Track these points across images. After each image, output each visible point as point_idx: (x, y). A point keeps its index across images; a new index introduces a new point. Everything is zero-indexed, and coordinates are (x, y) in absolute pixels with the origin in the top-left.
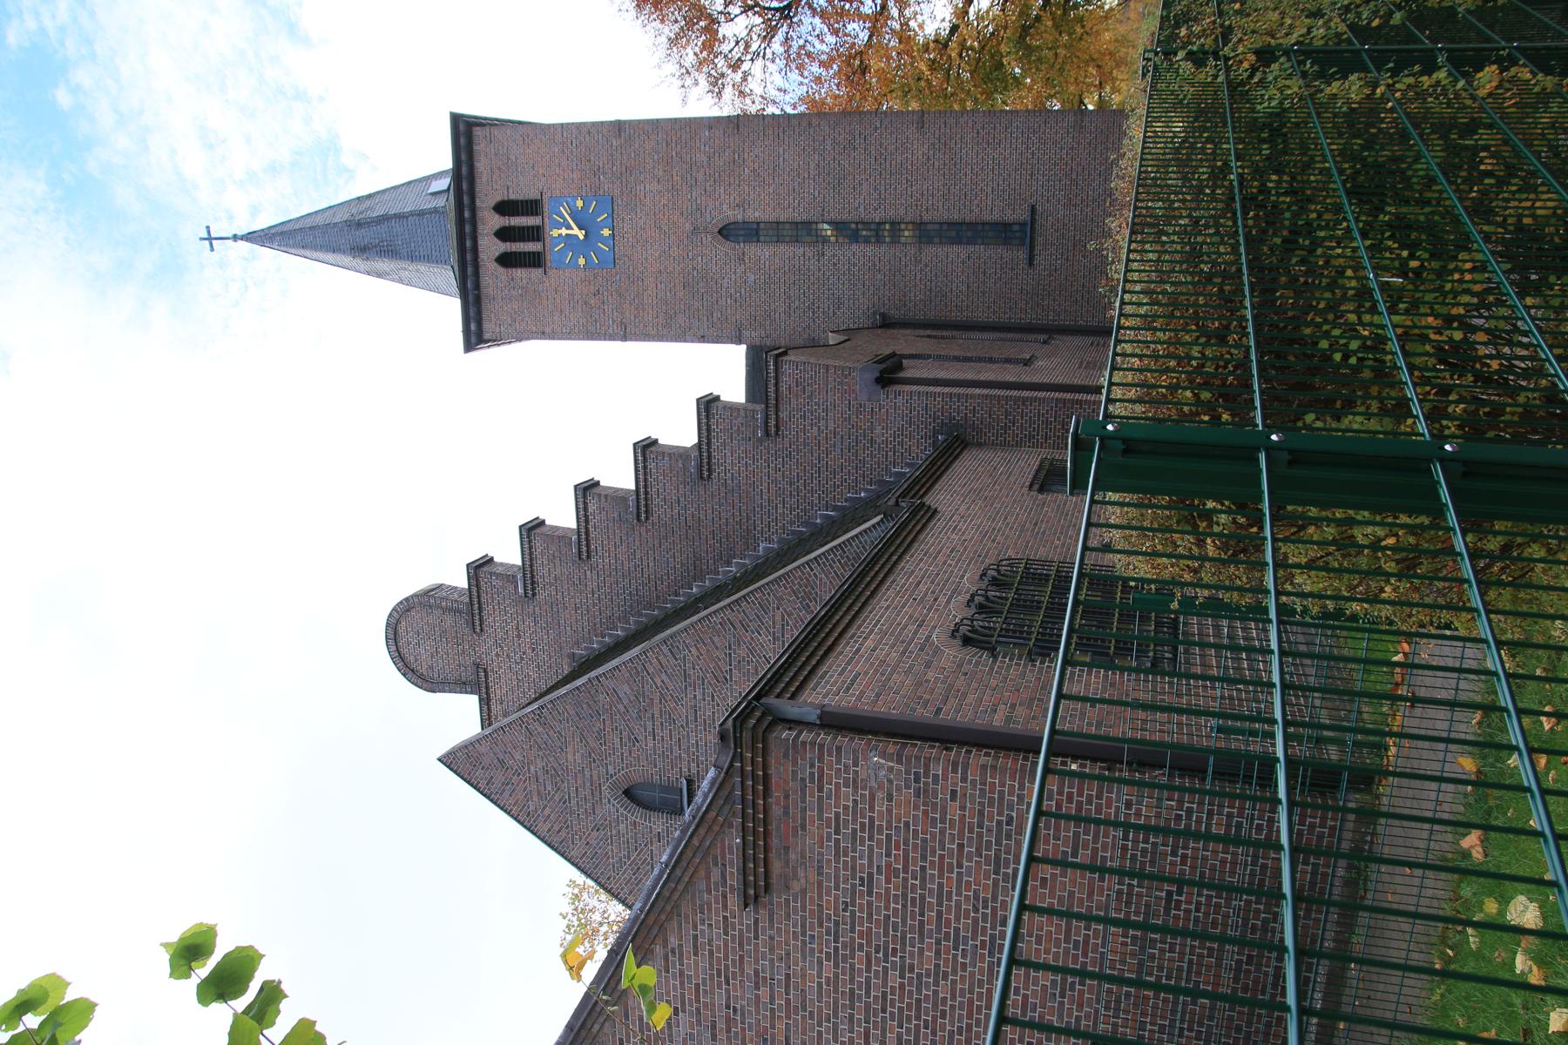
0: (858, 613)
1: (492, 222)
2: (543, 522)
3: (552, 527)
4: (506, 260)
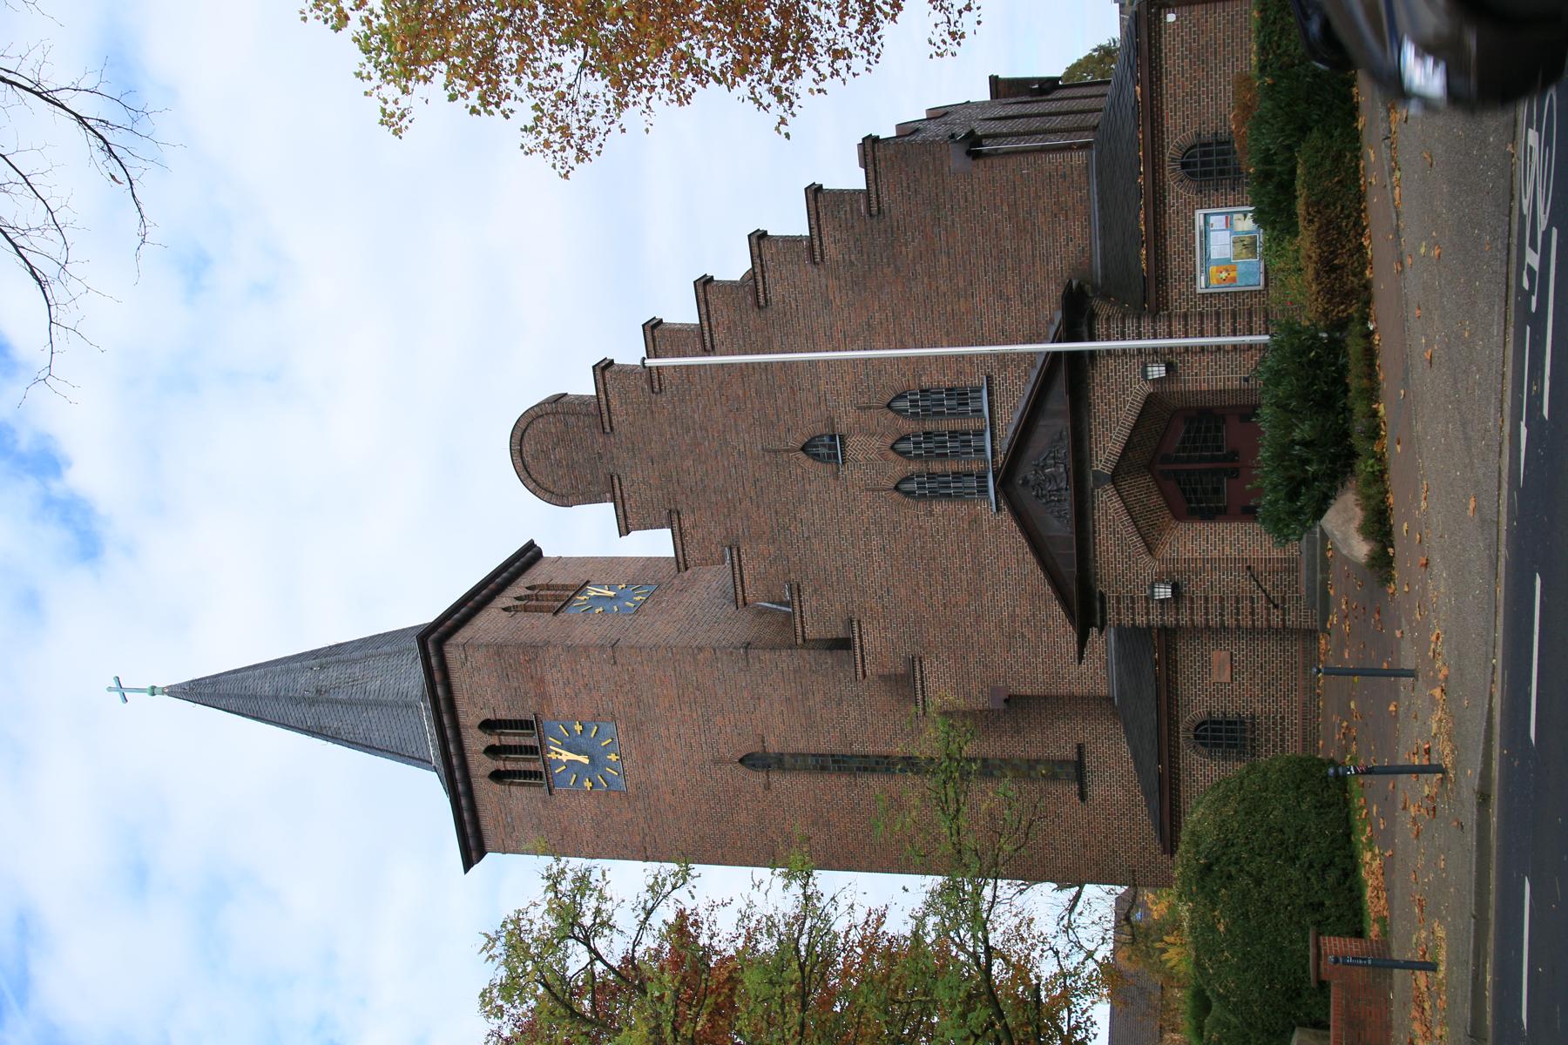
0: (733, 568)
1: (476, 742)
2: (612, 362)
3: (618, 365)
4: (497, 776)
